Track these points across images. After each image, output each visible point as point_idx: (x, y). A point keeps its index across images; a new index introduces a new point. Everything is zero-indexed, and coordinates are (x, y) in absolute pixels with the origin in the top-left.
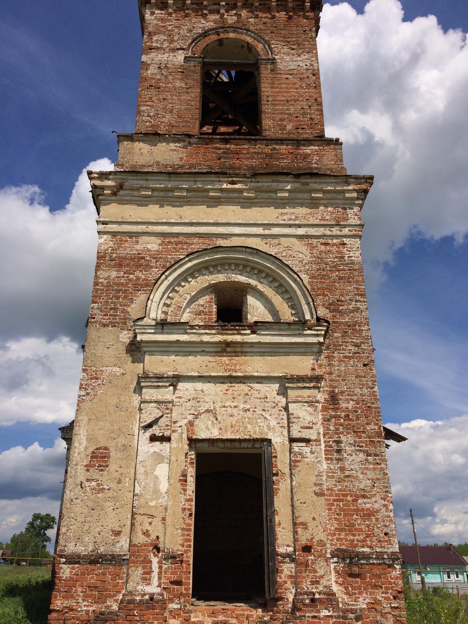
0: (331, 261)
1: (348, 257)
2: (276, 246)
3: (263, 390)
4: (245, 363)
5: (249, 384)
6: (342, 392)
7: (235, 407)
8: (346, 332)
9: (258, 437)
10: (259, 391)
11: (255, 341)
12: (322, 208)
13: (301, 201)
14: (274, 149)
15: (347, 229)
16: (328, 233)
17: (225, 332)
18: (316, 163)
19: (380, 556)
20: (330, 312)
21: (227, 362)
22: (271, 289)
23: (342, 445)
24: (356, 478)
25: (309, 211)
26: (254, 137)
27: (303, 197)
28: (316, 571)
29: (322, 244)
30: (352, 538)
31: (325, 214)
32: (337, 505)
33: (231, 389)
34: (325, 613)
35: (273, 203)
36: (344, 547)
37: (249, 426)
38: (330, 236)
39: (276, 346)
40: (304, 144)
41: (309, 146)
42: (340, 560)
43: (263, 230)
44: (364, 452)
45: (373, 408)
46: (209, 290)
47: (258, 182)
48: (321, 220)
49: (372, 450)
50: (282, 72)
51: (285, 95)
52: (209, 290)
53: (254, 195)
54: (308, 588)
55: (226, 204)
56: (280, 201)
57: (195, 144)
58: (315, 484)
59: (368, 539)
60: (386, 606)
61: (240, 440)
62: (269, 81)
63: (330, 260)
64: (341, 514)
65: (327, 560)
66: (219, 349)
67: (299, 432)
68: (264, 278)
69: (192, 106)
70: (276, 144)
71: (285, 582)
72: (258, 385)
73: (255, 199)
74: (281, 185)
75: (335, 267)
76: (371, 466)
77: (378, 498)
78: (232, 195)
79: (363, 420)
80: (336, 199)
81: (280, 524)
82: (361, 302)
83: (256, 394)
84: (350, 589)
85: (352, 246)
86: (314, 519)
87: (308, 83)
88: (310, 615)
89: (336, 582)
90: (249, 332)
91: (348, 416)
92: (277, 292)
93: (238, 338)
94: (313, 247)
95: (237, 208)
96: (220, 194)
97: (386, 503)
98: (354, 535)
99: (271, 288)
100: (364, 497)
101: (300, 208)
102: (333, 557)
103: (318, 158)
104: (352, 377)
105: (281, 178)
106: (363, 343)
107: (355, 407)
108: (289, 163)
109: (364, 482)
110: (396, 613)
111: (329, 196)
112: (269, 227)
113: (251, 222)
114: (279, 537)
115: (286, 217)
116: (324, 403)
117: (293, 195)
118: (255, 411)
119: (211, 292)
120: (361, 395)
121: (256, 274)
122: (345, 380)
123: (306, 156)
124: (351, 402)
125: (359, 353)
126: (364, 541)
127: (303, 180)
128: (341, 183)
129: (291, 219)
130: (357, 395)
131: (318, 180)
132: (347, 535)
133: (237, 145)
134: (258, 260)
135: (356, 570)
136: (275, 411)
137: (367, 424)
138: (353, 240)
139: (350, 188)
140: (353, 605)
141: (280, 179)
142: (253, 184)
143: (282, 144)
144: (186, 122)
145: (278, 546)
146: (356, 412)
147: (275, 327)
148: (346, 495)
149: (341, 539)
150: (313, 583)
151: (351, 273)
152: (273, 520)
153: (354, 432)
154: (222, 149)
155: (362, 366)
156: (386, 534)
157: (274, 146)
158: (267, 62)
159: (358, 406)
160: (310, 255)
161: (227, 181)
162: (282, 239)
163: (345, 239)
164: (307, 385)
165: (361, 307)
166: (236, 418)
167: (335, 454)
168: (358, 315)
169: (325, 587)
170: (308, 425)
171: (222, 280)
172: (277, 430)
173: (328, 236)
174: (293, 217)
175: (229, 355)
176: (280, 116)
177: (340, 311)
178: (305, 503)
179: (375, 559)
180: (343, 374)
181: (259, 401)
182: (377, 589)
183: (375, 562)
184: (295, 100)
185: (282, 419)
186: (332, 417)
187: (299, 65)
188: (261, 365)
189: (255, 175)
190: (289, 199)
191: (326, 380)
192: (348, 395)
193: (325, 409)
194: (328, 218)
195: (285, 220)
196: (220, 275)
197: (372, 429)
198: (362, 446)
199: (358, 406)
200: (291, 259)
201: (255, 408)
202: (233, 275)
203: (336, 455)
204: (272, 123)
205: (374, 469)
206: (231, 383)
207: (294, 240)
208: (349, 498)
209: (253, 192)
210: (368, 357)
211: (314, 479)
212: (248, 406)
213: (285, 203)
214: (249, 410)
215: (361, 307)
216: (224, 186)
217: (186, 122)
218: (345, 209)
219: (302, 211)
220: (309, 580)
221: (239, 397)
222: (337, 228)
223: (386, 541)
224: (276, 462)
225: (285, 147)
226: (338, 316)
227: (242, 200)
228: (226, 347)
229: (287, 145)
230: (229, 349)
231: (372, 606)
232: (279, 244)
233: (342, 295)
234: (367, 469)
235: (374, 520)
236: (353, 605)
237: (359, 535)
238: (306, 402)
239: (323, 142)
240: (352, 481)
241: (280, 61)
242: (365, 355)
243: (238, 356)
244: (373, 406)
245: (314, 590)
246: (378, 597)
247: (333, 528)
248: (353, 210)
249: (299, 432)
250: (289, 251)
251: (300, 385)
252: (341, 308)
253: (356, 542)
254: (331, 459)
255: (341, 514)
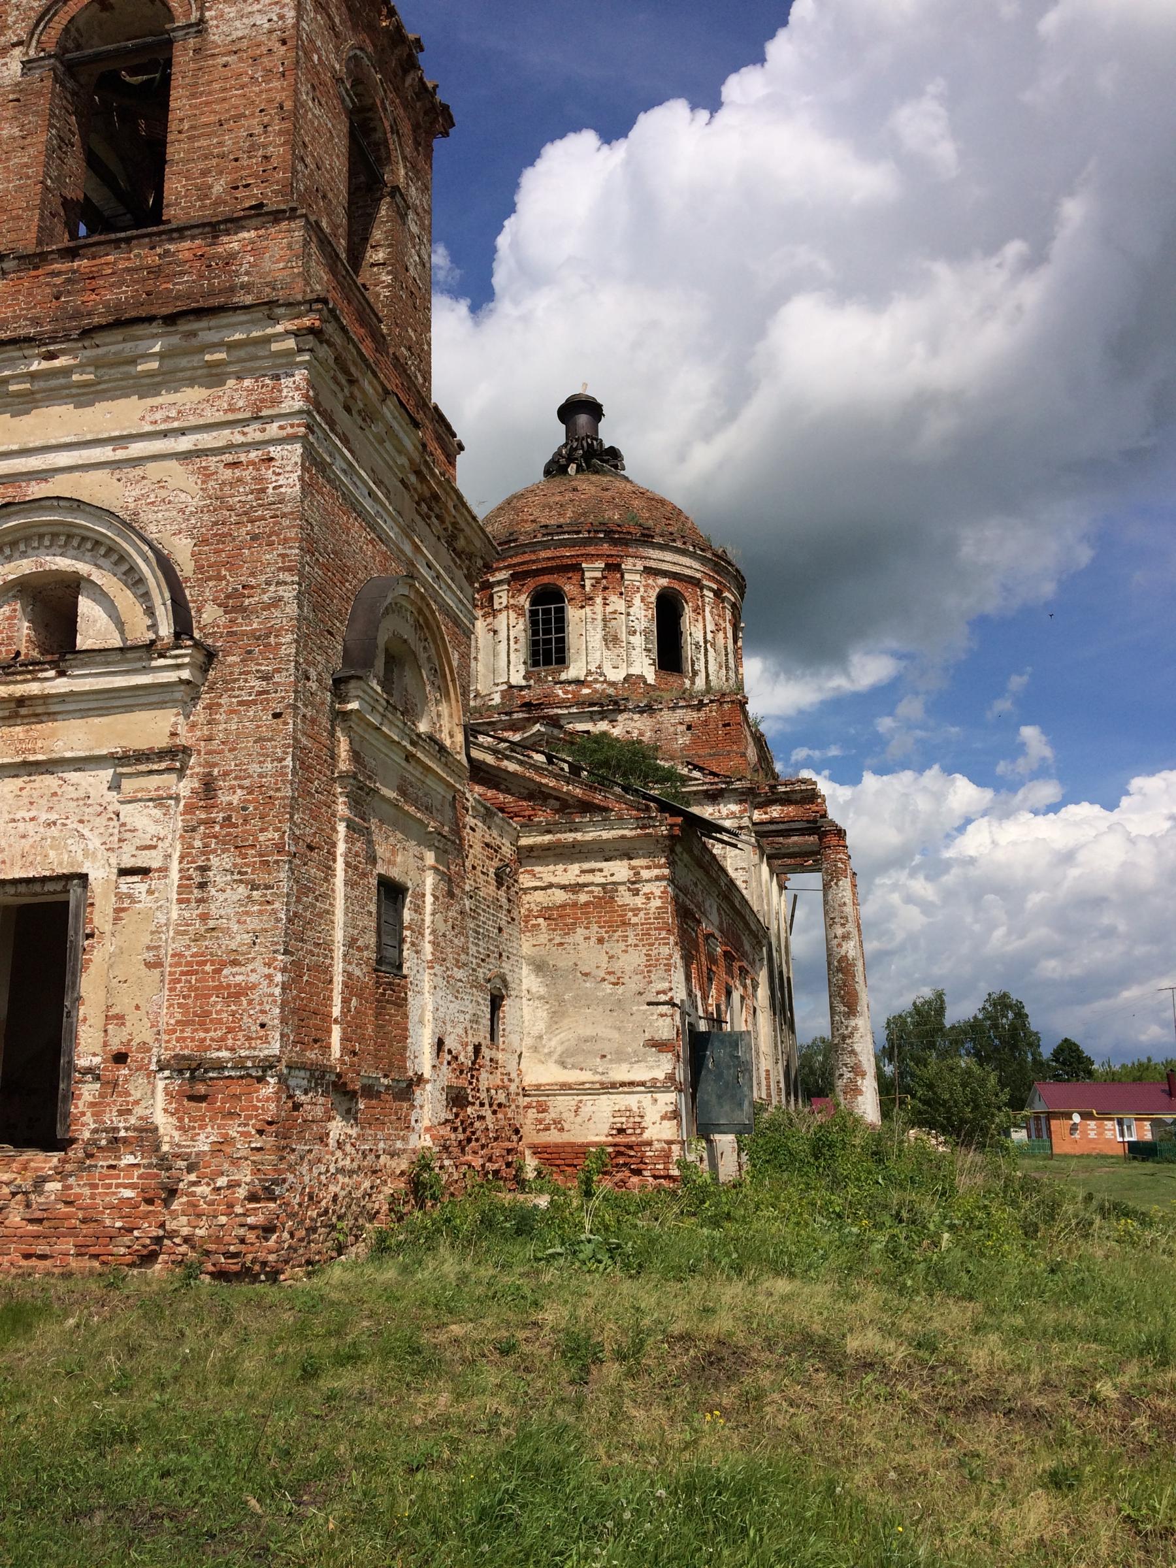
0: (240, 501)
1: (274, 488)
2: (137, 482)
3: (84, 783)
4: (53, 734)
5: (60, 775)
6: (226, 774)
7: (32, 819)
8: (250, 652)
9: (65, 871)
10: (76, 786)
11: (63, 690)
12: (231, 382)
13: (188, 374)
14: (167, 252)
15: (275, 425)
16: (238, 439)
17: (10, 678)
18: (247, 273)
19: (239, 1064)
20: (226, 612)
21: (21, 736)
22: (115, 579)
23: (211, 874)
24: (227, 931)
25: (202, 393)
26: (123, 235)
27: (190, 365)
28: (128, 1094)
29: (228, 465)
30: (202, 1035)
31: (236, 395)
32: (187, 981)
33: (28, 786)
34: (129, 1159)
35: (134, 386)
36: (186, 1052)
37: (52, 854)
38: (243, 445)
39: (106, 696)
40: (227, 230)
41: (236, 233)
42: (175, 1074)
43: (114, 450)
44: (246, 883)
45: (278, 799)
46: (10, 594)
47: (98, 346)
48: (226, 411)
49: (262, 878)
50: (216, 51)
51: (217, 107)
52: (10, 594)
53: (92, 377)
54: (112, 1121)
55: (47, 403)
56: (147, 381)
57: (14, 272)
58: (149, 948)
59: (229, 1036)
60: (241, 1148)
61: (44, 880)
62: (187, 81)
63: (237, 499)
64: (189, 996)
65: (150, 1075)
66: (7, 713)
67: (133, 856)
68: (104, 556)
69: (29, 178)
70: (171, 240)
71: (83, 1114)
72: (78, 774)
73: (99, 383)
74: (142, 346)
75: (246, 513)
76: (256, 908)
77: (257, 964)
78: (53, 383)
79: (256, 822)
80: (257, 358)
81: (85, 1019)
82: (286, 583)
83: (70, 792)
84: (186, 1120)
85: (285, 462)
86: (137, 1007)
87: (269, 65)
88: (105, 1164)
89: (165, 1110)
90: (52, 673)
91: (230, 817)
92: (126, 584)
93: (34, 688)
94: (208, 476)
95: (65, 411)
96: (28, 386)
97: (271, 971)
98: (207, 1031)
99: (115, 575)
100: (235, 963)
101: (189, 390)
102: (161, 1070)
103: (252, 259)
104: (248, 742)
105: (139, 330)
106: (278, 671)
107: (245, 801)
108: (194, 282)
109: (238, 938)
110: (257, 1157)
111: (242, 353)
112: (123, 443)
113: (89, 437)
114: (82, 1041)
115: (158, 416)
116: (190, 798)
117: (170, 364)
118: (64, 825)
119: (14, 596)
120: (261, 776)
121: (92, 550)
122: (234, 749)
123: (230, 259)
124: (239, 791)
125: (267, 692)
126: (223, 1039)
127: (185, 326)
128: (260, 320)
129: (168, 417)
130: (250, 776)
131: (213, 323)
132: (196, 1030)
133: (94, 258)
134: (83, 522)
135: (201, 1089)
136: (102, 820)
137: (262, 830)
138: (289, 447)
139: (280, 328)
140: (188, 1146)
141: (140, 333)
142: (88, 353)
143: (182, 238)
144: (13, 219)
145: (79, 1056)
146: (244, 809)
147: (98, 659)
148: (204, 963)
149: (184, 1039)
150: (121, 1113)
151: (275, 524)
152: (73, 1013)
153: (236, 847)
154: (66, 273)
155: (270, 717)
156: (263, 1026)
157: (168, 246)
158: (187, 34)
159: (250, 797)
160: (201, 493)
161: (38, 355)
162: (151, 466)
163: (272, 449)
164: (155, 767)
165: (286, 594)
166: (31, 841)
167: (196, 891)
168: (277, 613)
169: (141, 1118)
170: (150, 843)
171: (28, 572)
172: (100, 856)
173: (239, 446)
174: (173, 414)
175: (25, 721)
176: (202, 165)
177: (245, 610)
178: (125, 982)
179: (232, 1068)
180: (232, 738)
181: (75, 803)
182: (232, 1119)
183: (233, 1074)
184: (237, 118)
185: (111, 835)
186: (202, 822)
187: (254, 25)
188: (80, 736)
189: (86, 333)
190: (164, 374)
191: (199, 754)
192: (236, 778)
193: (190, 809)
194: (241, 404)
195: (156, 422)
196: (25, 561)
197: (269, 840)
198: (246, 873)
199: (250, 797)
200: (164, 508)
201: (67, 818)
202: (48, 558)
203: (197, 894)
204: (184, 186)
205: (261, 912)
206: (30, 775)
207: (173, 464)
208: (208, 968)
209: (92, 369)
210: (283, 698)
211: (146, 939)
212: (53, 816)
213: (159, 384)
214: (55, 823)
215: (286, 594)
216: (35, 366)
217: (13, 219)
218: (277, 377)
219: (192, 395)
220: (115, 1109)
221: (40, 801)
222: (256, 425)
223: (260, 1038)
224: (91, 913)
225: (187, 244)
226: (240, 620)
227: (74, 391)
228: (19, 707)
229: (193, 238)
230: (23, 711)
231: (219, 1147)
232: (143, 478)
233: (252, 574)
234: (247, 913)
235: (245, 1002)
236: (188, 1146)
237: (215, 1030)
238: (151, 800)
239: (264, 219)
240: (218, 938)
241: (215, 22)
242: (278, 695)
243: (42, 722)
244: (278, 794)
245: (121, 1125)
246: (230, 1132)
247: (172, 1021)
248: (292, 379)
249: (133, 856)
250: (161, 491)
251: (143, 768)
252: (247, 602)
253: (208, 1042)
254: (188, 901)
255: (189, 996)
